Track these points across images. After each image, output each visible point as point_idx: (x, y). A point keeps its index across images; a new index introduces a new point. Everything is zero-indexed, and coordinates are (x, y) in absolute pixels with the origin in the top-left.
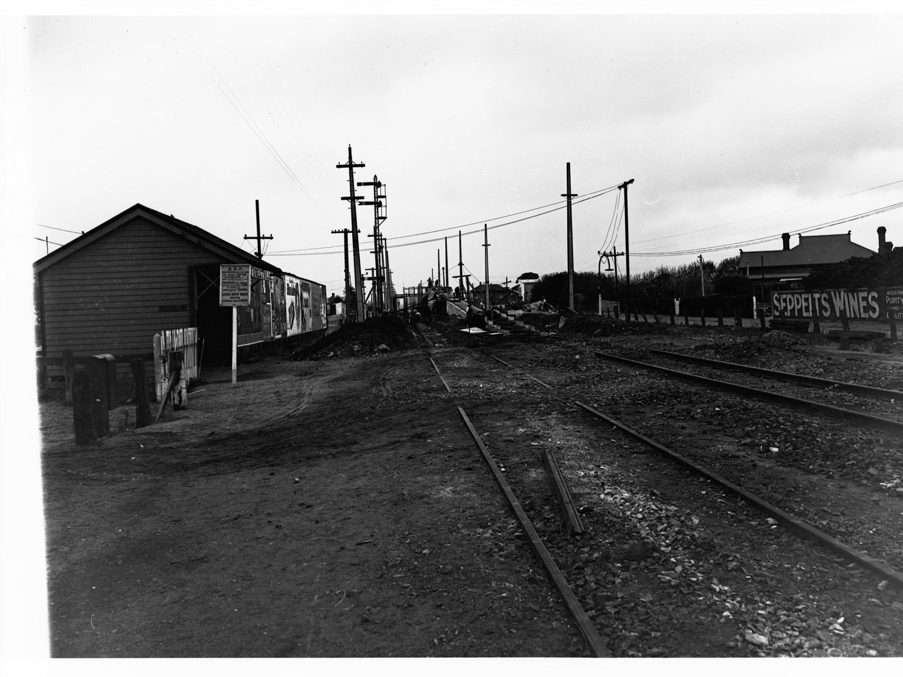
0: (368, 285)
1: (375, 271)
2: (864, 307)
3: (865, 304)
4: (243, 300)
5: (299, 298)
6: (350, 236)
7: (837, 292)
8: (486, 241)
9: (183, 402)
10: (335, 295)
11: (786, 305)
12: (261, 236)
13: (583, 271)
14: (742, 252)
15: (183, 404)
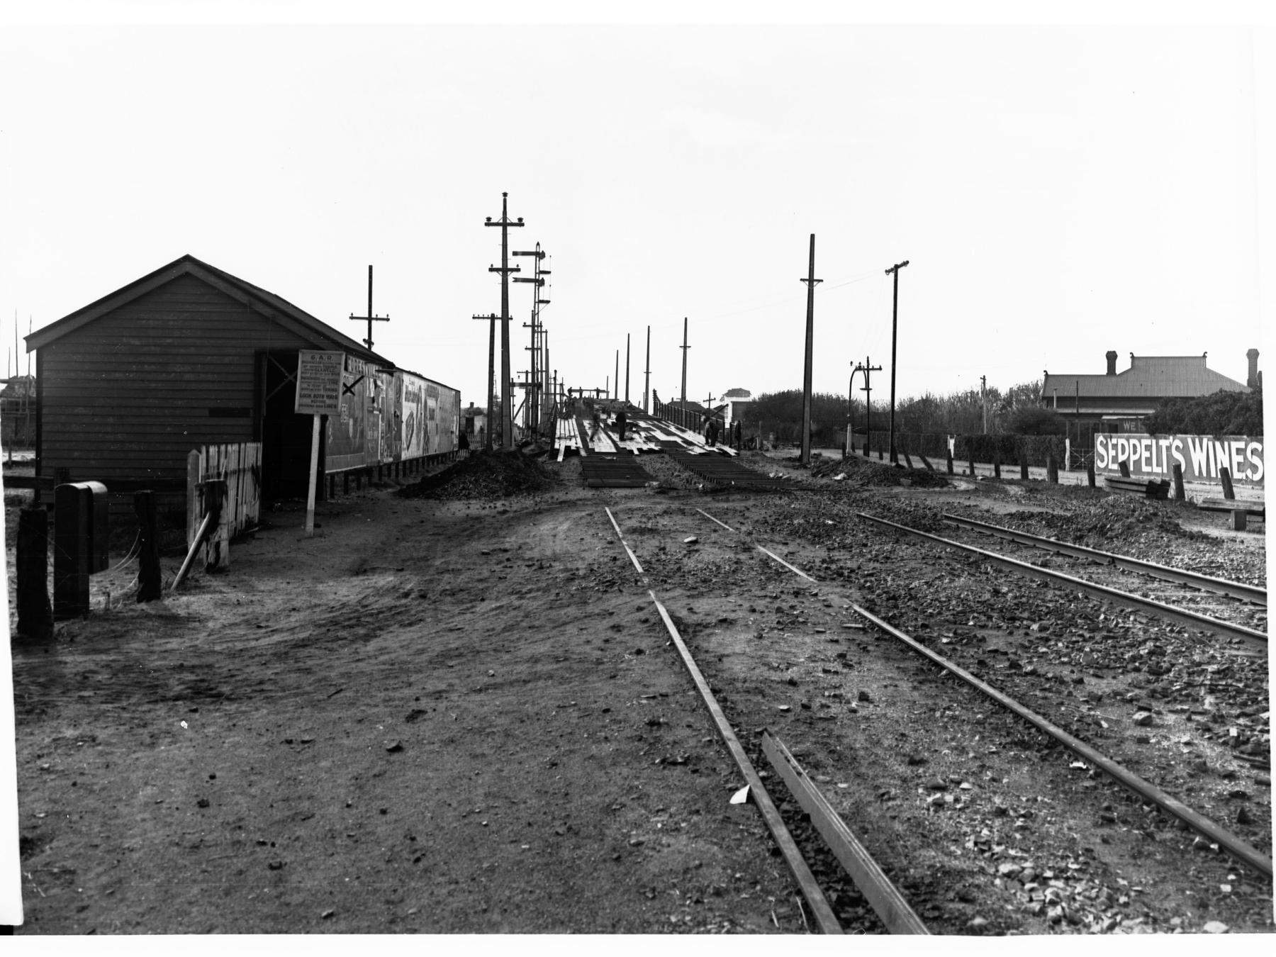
0: (519, 395)
1: (530, 375)
2: (1239, 464)
3: (1241, 459)
4: (330, 406)
6: (498, 324)
7: (1197, 440)
8: (685, 342)
9: (221, 560)
10: (475, 406)
12: (374, 316)
14: (1047, 375)
15: (221, 564)
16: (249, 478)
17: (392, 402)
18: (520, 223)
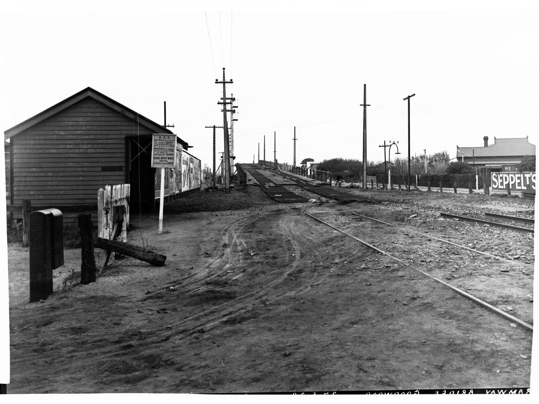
4: (170, 163)
5: (188, 167)
11: (503, 181)
13: (333, 158)
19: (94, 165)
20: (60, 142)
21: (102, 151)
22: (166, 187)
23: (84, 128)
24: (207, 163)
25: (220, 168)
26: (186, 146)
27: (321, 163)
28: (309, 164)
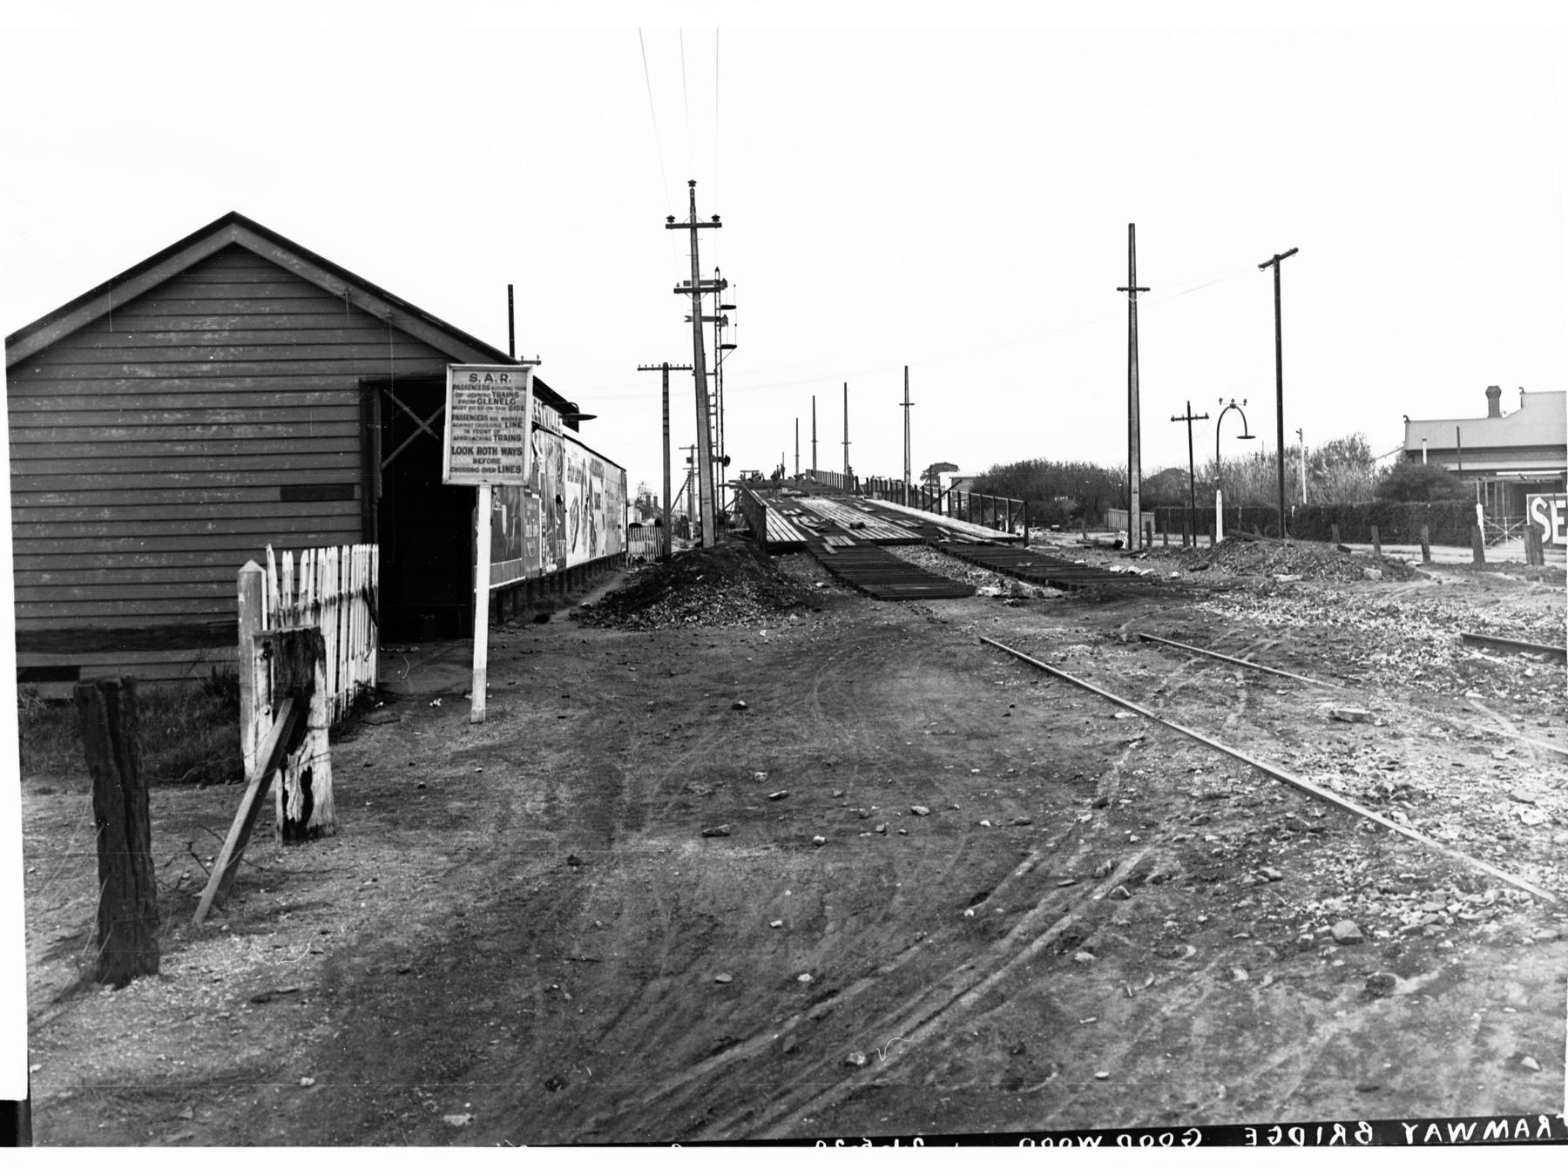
1: (696, 451)
2: (1560, 526)
4: (508, 469)
8: (907, 398)
9: (315, 811)
13: (1020, 461)
15: (316, 818)
16: (359, 611)
17: (553, 481)
18: (716, 223)
19: (252, 479)
20: (138, 404)
21: (281, 430)
22: (500, 550)
23: (220, 354)
24: (645, 478)
25: (685, 493)
26: (572, 416)
27: (984, 476)
28: (945, 480)
